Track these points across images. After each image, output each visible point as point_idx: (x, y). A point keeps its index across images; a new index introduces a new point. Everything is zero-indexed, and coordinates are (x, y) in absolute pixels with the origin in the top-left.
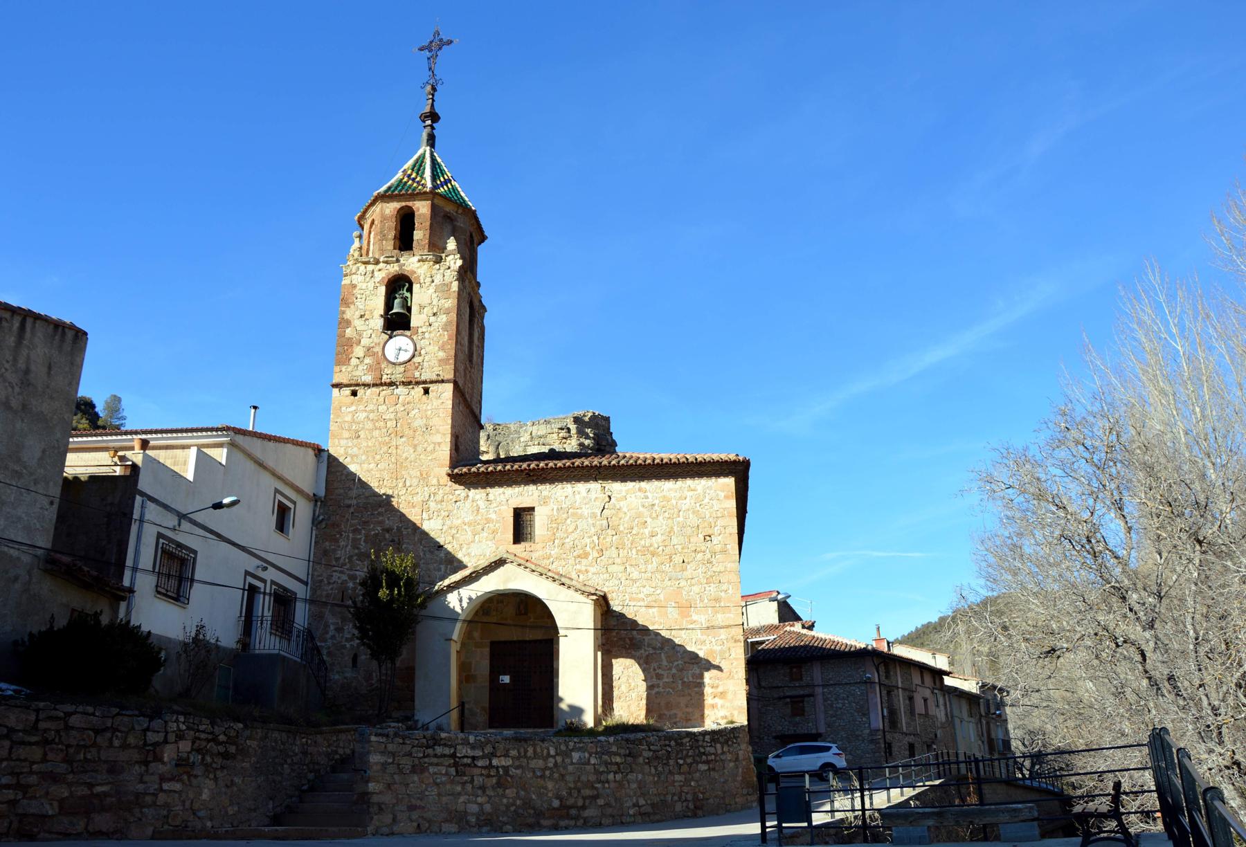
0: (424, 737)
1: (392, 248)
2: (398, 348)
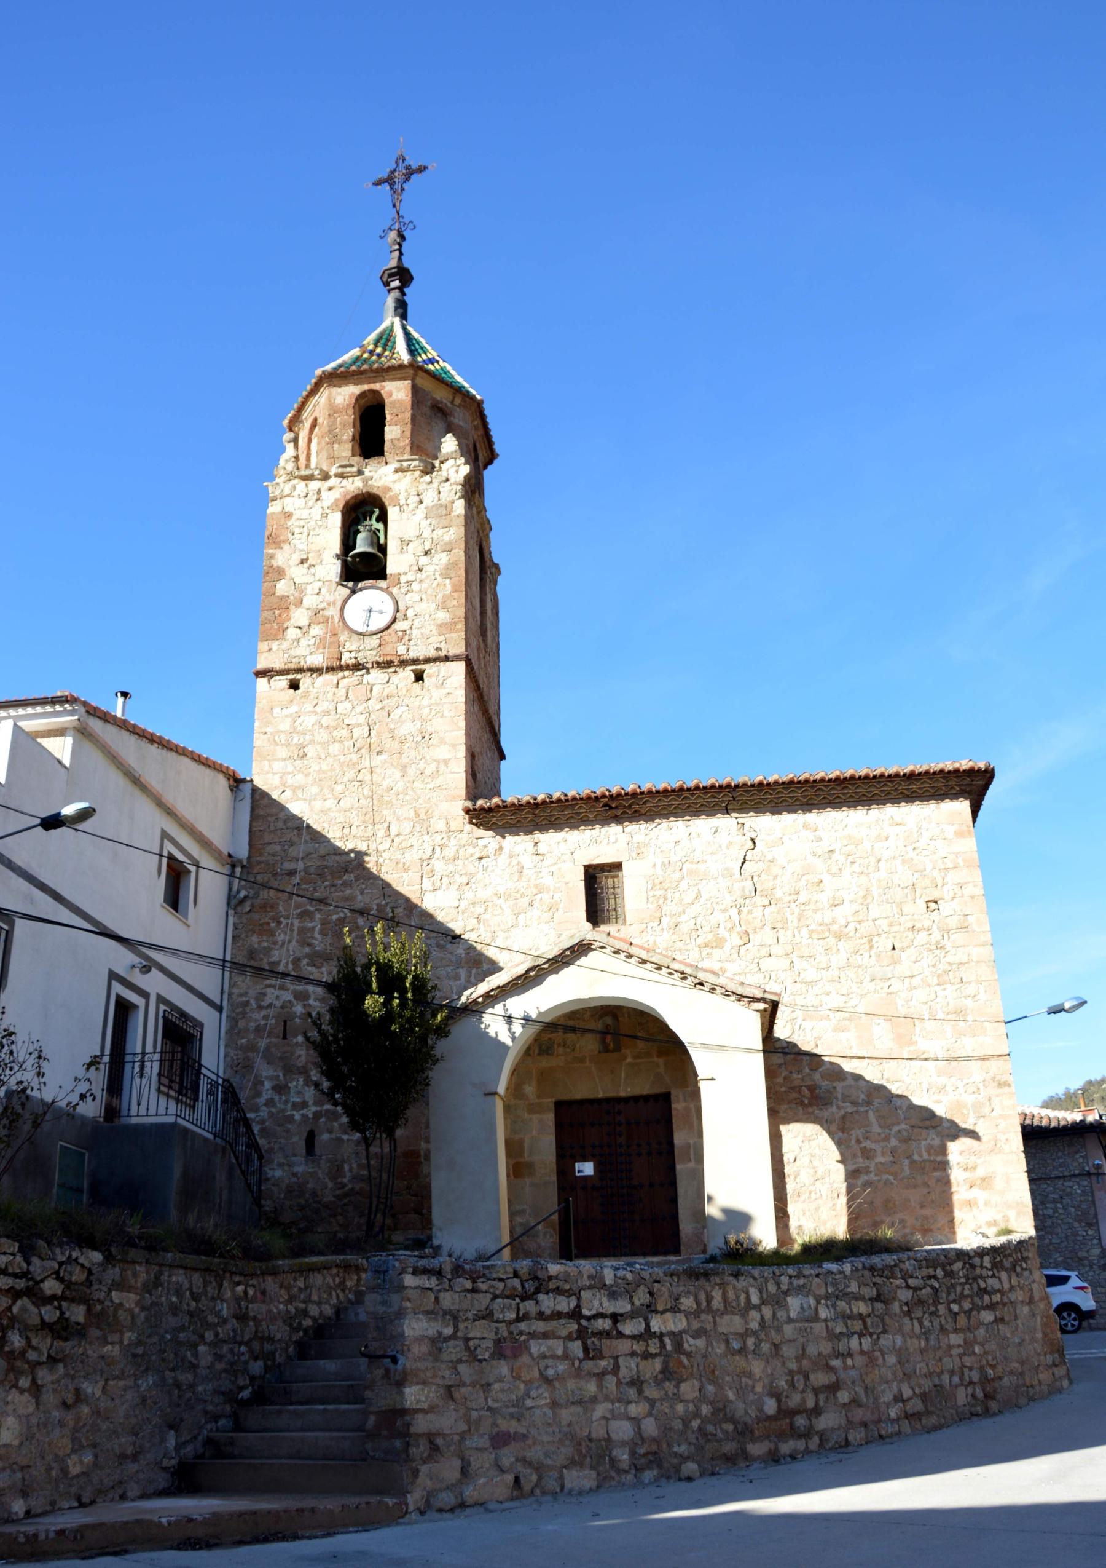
0: (516, 1275)
1: (350, 453)
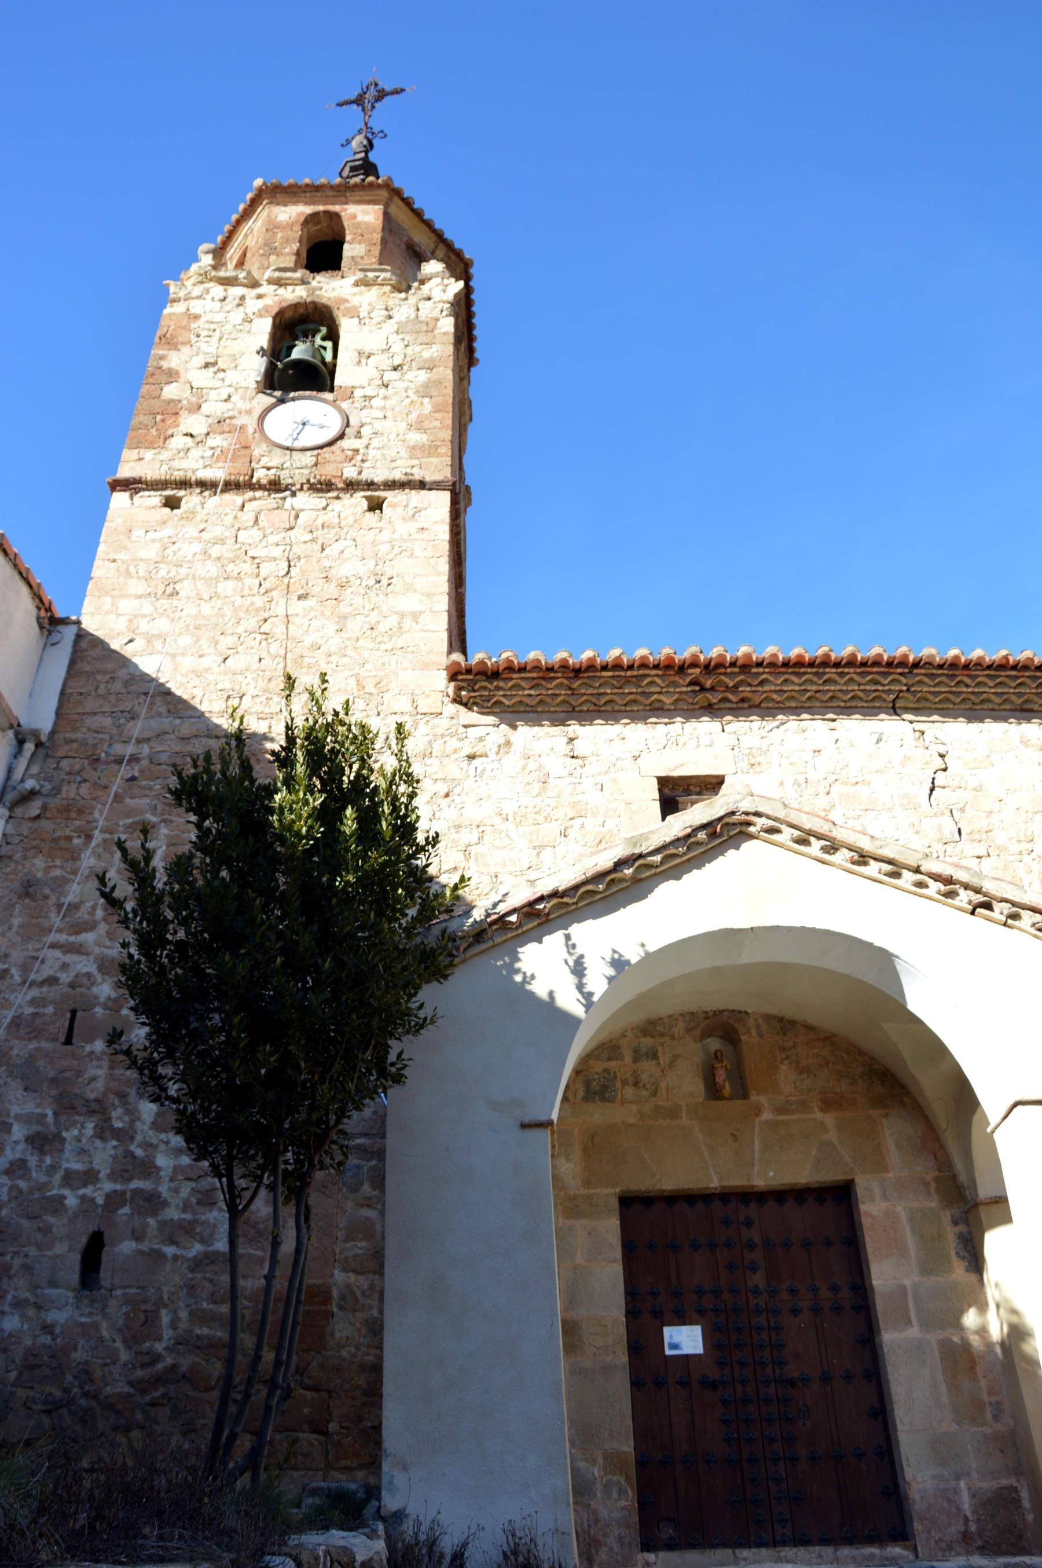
2: (299, 420)
